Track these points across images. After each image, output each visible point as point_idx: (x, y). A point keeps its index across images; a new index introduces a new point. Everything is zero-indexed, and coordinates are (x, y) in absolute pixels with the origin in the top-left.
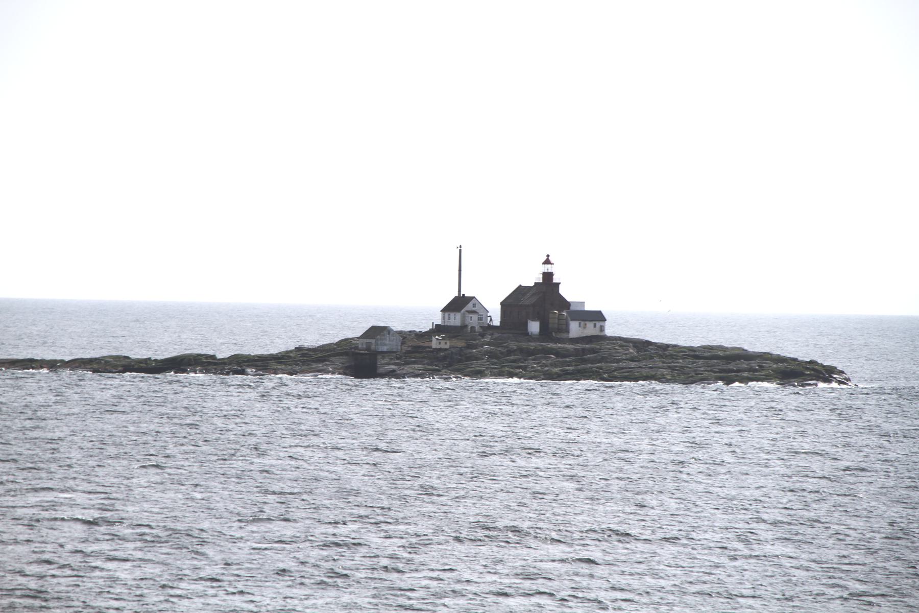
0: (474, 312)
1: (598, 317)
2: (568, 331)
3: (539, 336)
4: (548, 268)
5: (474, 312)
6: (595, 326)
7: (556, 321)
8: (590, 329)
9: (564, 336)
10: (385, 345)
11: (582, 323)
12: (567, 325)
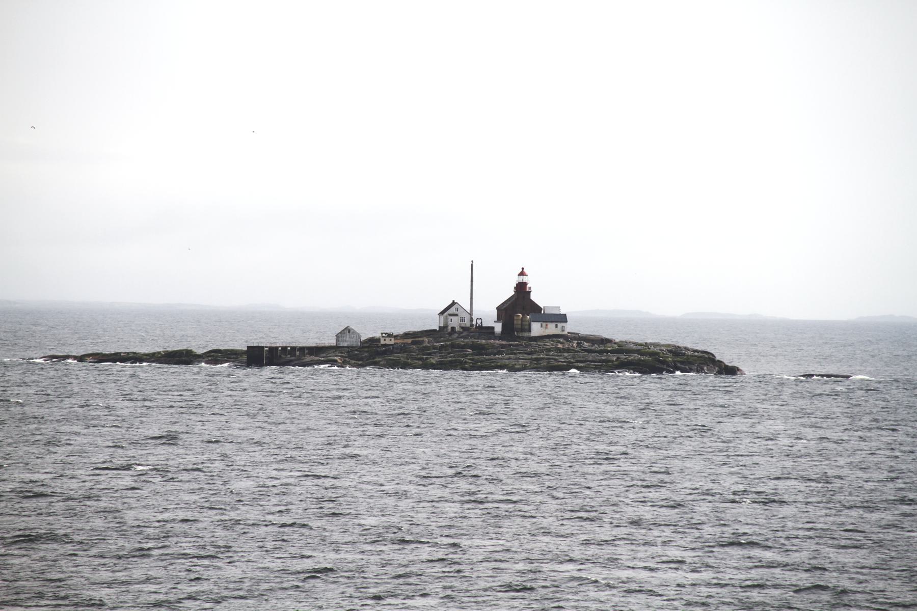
0: (456, 315)
1: (562, 318)
2: (530, 330)
3: (513, 336)
4: (521, 279)
5: (456, 315)
6: (557, 326)
7: (520, 322)
8: (552, 329)
9: (526, 334)
10: (346, 341)
11: (544, 324)
12: (530, 325)
